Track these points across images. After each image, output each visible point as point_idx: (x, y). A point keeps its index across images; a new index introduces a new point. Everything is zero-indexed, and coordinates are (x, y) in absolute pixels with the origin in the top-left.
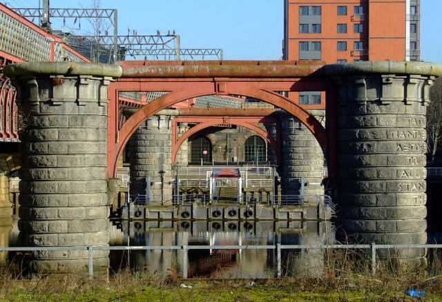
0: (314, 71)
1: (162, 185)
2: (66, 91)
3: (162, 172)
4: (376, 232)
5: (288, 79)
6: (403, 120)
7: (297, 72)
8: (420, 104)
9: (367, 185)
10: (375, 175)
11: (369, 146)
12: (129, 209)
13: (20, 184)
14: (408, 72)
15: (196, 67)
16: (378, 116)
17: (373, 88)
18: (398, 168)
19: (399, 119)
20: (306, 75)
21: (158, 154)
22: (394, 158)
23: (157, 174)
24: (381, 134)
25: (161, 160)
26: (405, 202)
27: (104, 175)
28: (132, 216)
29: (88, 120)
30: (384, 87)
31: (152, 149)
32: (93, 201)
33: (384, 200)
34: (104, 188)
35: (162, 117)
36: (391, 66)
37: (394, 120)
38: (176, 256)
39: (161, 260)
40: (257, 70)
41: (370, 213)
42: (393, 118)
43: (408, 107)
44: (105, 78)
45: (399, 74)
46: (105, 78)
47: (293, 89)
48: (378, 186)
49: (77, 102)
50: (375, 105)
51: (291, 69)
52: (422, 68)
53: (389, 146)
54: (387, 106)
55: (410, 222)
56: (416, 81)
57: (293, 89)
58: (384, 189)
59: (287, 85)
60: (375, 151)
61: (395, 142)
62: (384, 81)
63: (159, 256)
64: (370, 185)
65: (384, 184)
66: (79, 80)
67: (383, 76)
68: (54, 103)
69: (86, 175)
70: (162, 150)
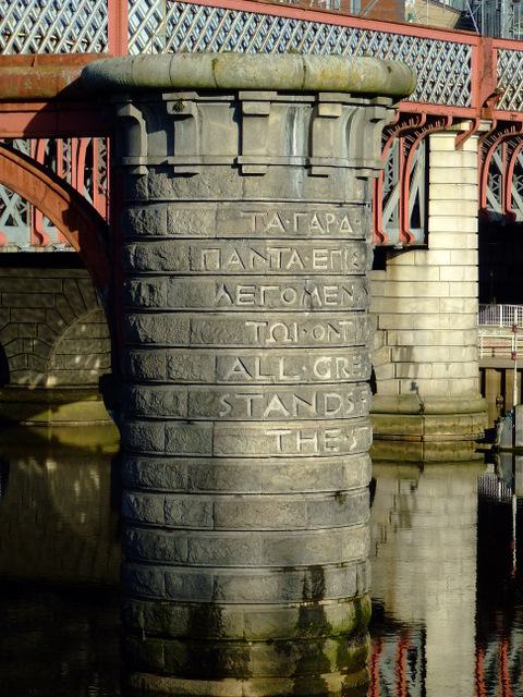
0: (69, 82)
2: (208, 133)
4: (164, 528)
5: (14, 107)
6: (236, 218)
7: (28, 86)
8: (299, 173)
9: (147, 397)
10: (164, 373)
11: (151, 289)
12: (514, 423)
14: (313, 86)
16: (170, 207)
17: (158, 130)
18: (221, 352)
19: (222, 216)
20: (51, 93)
22: (208, 322)
24: (177, 256)
30: (179, 126)
36: (174, 68)
41: (152, 476)
42: (204, 212)
44: (322, 97)
45: (209, 92)
46: (242, 95)
47: (31, 133)
48: (169, 401)
49: (308, 166)
50: (163, 176)
51: (14, 77)
52: (266, 71)
53: (194, 291)
54: (193, 179)
55: (258, 502)
56: (338, 110)
57: (31, 133)
58: (183, 408)
60: (163, 306)
61: (212, 280)
62: (170, 108)
64: (154, 396)
65: (183, 397)
66: (237, 104)
67: (165, 96)
68: (177, 170)
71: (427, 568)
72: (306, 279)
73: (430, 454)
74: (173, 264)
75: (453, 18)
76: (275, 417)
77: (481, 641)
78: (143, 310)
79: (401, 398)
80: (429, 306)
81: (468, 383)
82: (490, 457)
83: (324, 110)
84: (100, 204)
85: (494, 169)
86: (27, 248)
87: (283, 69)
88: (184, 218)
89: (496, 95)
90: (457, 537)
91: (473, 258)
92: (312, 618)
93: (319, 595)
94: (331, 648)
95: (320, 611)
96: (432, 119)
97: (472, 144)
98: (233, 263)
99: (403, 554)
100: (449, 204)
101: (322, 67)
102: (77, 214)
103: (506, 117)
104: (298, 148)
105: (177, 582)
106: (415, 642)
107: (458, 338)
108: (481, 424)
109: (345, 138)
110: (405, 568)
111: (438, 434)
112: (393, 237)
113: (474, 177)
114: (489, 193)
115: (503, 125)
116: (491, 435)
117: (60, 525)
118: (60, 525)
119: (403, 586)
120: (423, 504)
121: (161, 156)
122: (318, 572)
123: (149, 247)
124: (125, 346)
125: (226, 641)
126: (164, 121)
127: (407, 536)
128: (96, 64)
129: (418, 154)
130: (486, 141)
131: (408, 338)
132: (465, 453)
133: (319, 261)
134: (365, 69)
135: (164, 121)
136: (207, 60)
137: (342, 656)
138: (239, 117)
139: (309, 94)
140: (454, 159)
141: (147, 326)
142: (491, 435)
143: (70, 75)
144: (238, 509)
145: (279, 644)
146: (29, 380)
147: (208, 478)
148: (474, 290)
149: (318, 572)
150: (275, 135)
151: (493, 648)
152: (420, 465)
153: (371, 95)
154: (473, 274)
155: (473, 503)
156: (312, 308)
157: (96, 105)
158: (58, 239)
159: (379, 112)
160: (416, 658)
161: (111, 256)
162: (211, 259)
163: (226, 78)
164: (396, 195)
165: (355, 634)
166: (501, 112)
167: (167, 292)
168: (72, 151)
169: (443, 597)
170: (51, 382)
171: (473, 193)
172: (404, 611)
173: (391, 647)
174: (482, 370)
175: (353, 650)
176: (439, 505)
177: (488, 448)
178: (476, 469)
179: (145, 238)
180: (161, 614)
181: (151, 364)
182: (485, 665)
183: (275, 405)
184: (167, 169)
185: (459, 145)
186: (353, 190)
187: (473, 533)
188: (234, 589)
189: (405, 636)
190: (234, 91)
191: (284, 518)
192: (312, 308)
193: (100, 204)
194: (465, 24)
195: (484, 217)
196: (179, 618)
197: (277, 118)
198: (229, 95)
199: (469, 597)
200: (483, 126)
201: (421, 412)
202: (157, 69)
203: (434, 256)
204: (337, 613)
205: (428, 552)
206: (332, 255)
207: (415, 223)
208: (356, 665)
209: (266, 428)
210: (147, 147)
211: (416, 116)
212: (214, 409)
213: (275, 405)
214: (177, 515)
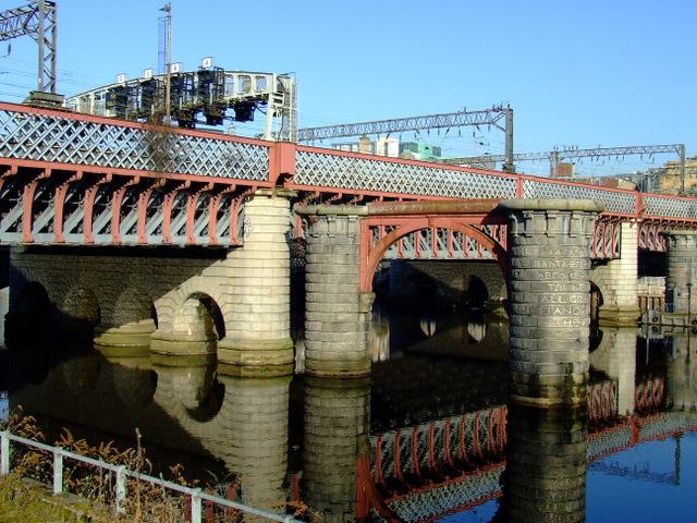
1: (689, 296)
2: (537, 223)
3: (689, 285)
13: (457, 290)
15: (434, 205)
21: (685, 269)
23: (684, 286)
25: (689, 274)
26: (245, 326)
27: (354, 290)
28: (650, 321)
29: (338, 248)
30: (528, 221)
31: (680, 265)
32: (341, 309)
33: (529, 322)
34: (353, 299)
35: (689, 237)
37: (537, 251)
38: (174, 355)
39: (688, 361)
40: (453, 208)
43: (550, 239)
45: (537, 210)
50: (523, 238)
56: (579, 216)
59: (478, 220)
63: (685, 357)
66: (546, 214)
69: (335, 290)
70: (690, 266)
71: (619, 360)
72: (568, 271)
73: (621, 324)
74: (526, 265)
75: (634, 186)
76: (558, 314)
77: (637, 384)
78: (515, 279)
79: (611, 306)
80: (621, 277)
81: (633, 301)
82: (640, 326)
83: (575, 216)
84: (505, 247)
85: (643, 234)
86: (476, 257)
87: (561, 203)
88: (528, 250)
89: (643, 210)
90: (629, 350)
91: (636, 262)
92: (568, 380)
93: (571, 372)
94: (575, 389)
95: (572, 378)
96: (622, 218)
97: (635, 226)
98: (545, 264)
99: (611, 355)
100: (117, 354)
101: (573, 203)
102: (497, 249)
103: (330, 190)
104: (566, 228)
105: (525, 367)
106: (615, 383)
107: (630, 288)
108: (638, 315)
109: (581, 225)
110: (613, 361)
111: (624, 318)
112: (609, 255)
113: (636, 236)
114: (641, 241)
115: (645, 220)
116: (640, 319)
117: (161, 475)
118: (161, 475)
119: (611, 365)
120: (618, 340)
121: (522, 231)
122: (571, 364)
123: (518, 260)
124: (511, 290)
125: (541, 386)
126: (523, 220)
127: (612, 350)
128: (502, 202)
129: (618, 229)
130: (640, 224)
131: (614, 287)
132: (632, 324)
133: (572, 265)
134: (588, 204)
135: (523, 220)
136: (536, 201)
137: (578, 392)
138: (547, 218)
139: (569, 211)
140: (630, 230)
141: (517, 284)
142: (640, 319)
143: (495, 205)
144: (545, 344)
145: (558, 387)
146: (494, 298)
147: (537, 333)
148: (636, 272)
149: (571, 364)
150: (558, 225)
151: (641, 386)
152: (618, 327)
153: (590, 212)
154: (636, 267)
155: (635, 340)
156: (570, 279)
157: (502, 215)
158: (489, 255)
159: (593, 217)
160: (615, 389)
161: (506, 259)
162: (537, 264)
163: (542, 206)
164: (610, 242)
165: (583, 384)
166: (645, 216)
167: (523, 274)
168: (492, 228)
169: (625, 371)
170: (501, 299)
171: (635, 241)
172: (611, 373)
173: (607, 385)
174: (640, 298)
175: (582, 390)
176: (623, 340)
177: (639, 323)
178: (635, 330)
179: (517, 256)
180: (520, 376)
181: (518, 297)
182: (638, 392)
183: (558, 310)
184: (524, 235)
185: (631, 226)
186: (584, 242)
187: (635, 349)
188: (544, 369)
189: (611, 381)
190: (545, 210)
191: (560, 347)
192: (570, 279)
193: (505, 247)
194: (637, 189)
195: (639, 249)
196: (526, 377)
197: (559, 219)
198: (543, 211)
199: (633, 370)
200: (639, 220)
201: (618, 311)
202: (520, 204)
203: (622, 261)
204: (577, 378)
205: (620, 355)
206: (578, 263)
207: (617, 250)
208: (583, 395)
209: (555, 318)
210: (518, 228)
211: (608, 216)
212: (540, 311)
213: (558, 310)
214: (525, 345)
